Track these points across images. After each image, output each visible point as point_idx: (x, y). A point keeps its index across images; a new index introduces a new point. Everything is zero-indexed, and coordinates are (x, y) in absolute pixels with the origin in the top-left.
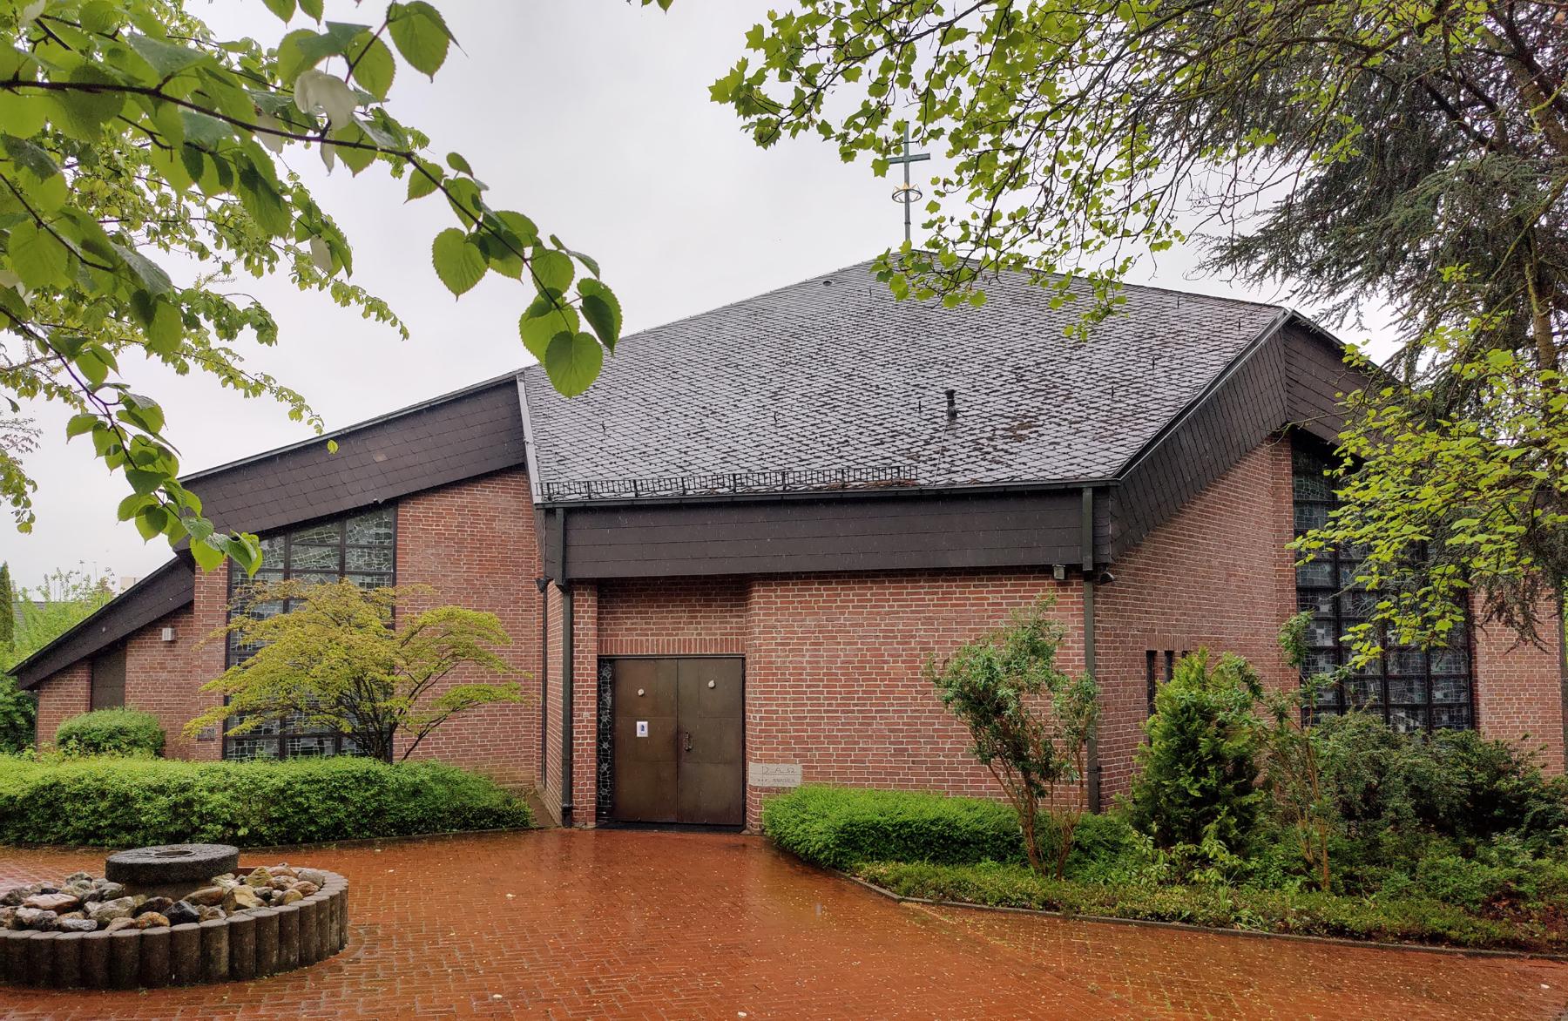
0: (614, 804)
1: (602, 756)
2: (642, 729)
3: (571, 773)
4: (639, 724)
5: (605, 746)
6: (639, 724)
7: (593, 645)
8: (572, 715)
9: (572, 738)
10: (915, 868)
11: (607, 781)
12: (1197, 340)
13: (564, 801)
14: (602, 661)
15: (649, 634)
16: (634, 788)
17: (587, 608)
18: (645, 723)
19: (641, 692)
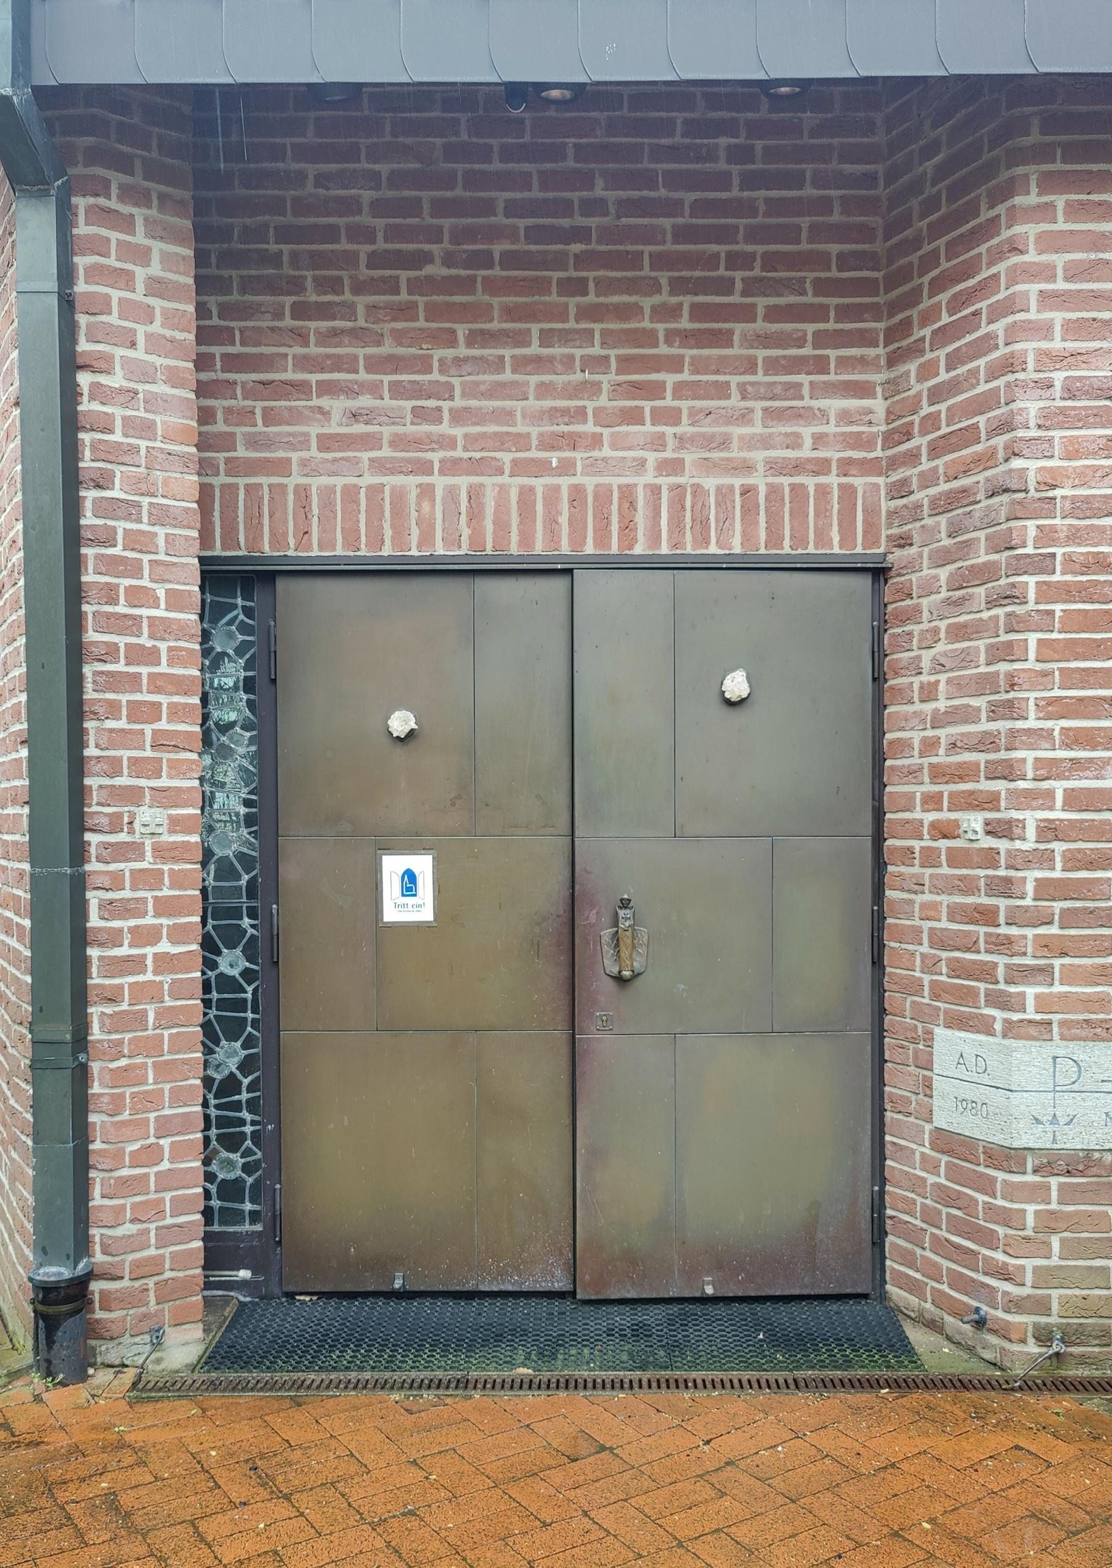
0: (275, 1222)
1: (226, 1011)
2: (407, 890)
3: (81, 1104)
4: (393, 866)
5: (232, 962)
6: (393, 866)
7: (179, 488)
8: (78, 824)
9: (80, 938)
10: (333, 1376)
11: (248, 1117)
12: (930, 858)
13: (44, 1251)
14: (234, 584)
15: (436, 451)
16: (378, 1157)
17: (143, 287)
18: (423, 865)
19: (401, 722)
